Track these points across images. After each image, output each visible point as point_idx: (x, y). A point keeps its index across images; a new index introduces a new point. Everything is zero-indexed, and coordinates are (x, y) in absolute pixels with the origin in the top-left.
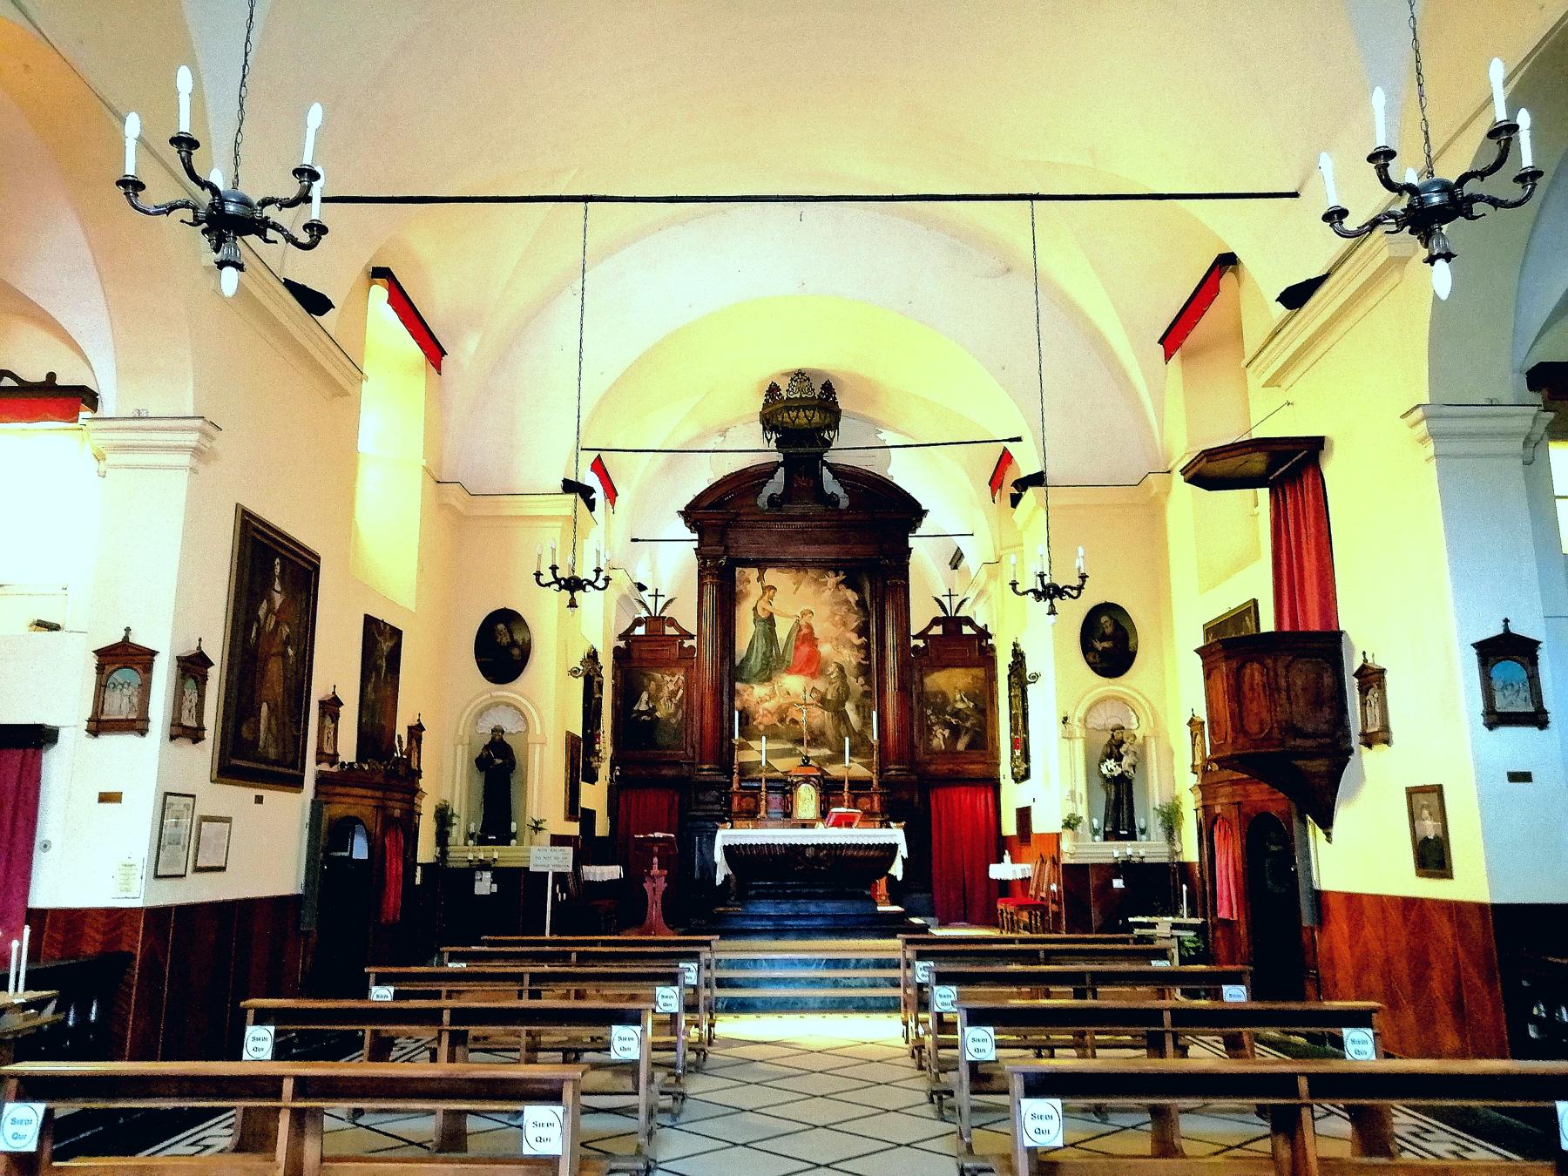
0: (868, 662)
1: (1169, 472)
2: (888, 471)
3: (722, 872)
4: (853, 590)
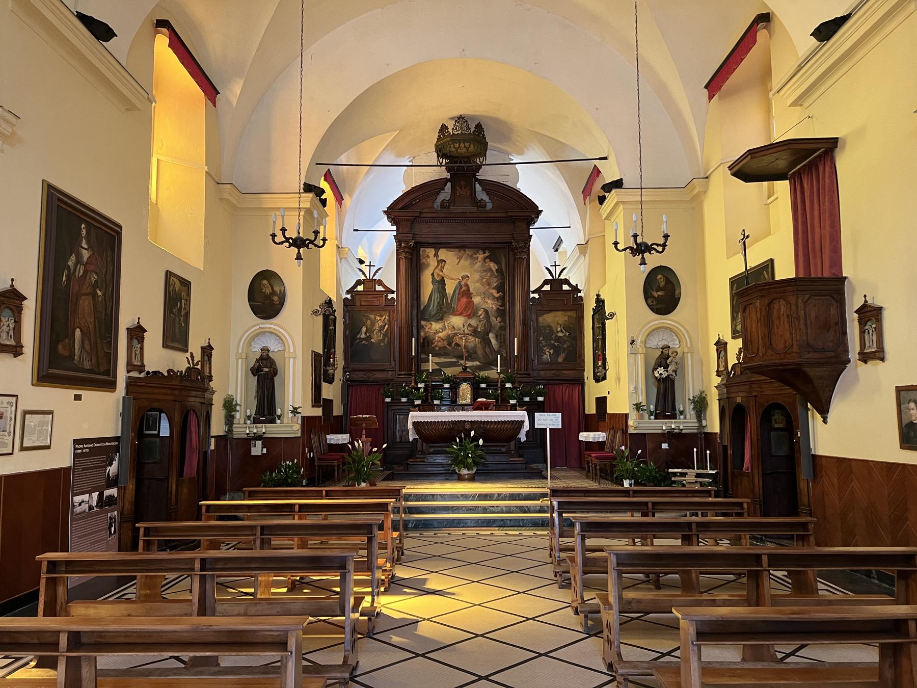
0: (503, 308)
1: (707, 178)
2: (517, 185)
4: (495, 262)
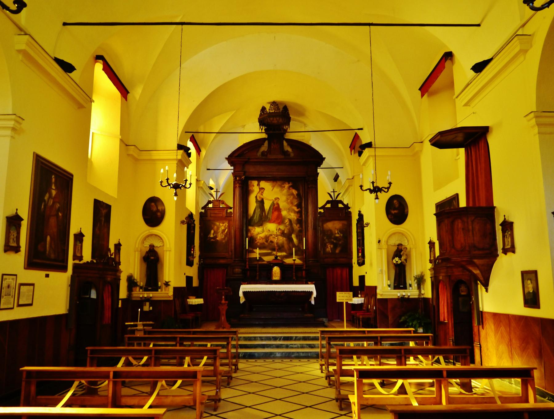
1: (422, 142)
3: (242, 300)
